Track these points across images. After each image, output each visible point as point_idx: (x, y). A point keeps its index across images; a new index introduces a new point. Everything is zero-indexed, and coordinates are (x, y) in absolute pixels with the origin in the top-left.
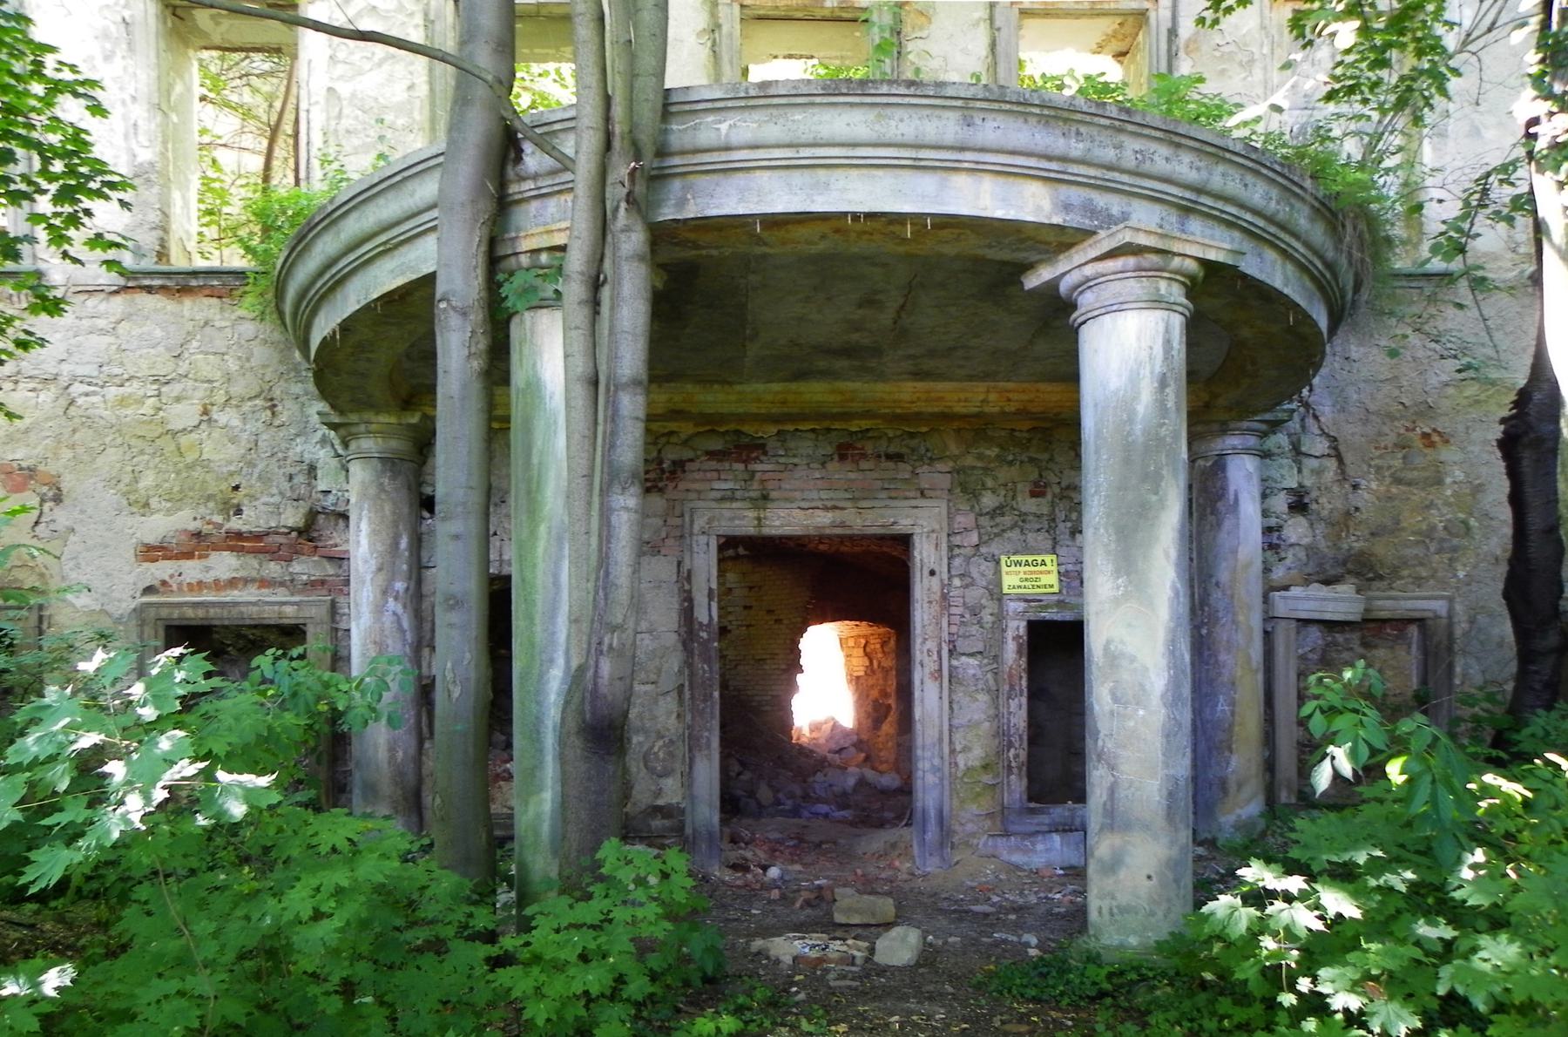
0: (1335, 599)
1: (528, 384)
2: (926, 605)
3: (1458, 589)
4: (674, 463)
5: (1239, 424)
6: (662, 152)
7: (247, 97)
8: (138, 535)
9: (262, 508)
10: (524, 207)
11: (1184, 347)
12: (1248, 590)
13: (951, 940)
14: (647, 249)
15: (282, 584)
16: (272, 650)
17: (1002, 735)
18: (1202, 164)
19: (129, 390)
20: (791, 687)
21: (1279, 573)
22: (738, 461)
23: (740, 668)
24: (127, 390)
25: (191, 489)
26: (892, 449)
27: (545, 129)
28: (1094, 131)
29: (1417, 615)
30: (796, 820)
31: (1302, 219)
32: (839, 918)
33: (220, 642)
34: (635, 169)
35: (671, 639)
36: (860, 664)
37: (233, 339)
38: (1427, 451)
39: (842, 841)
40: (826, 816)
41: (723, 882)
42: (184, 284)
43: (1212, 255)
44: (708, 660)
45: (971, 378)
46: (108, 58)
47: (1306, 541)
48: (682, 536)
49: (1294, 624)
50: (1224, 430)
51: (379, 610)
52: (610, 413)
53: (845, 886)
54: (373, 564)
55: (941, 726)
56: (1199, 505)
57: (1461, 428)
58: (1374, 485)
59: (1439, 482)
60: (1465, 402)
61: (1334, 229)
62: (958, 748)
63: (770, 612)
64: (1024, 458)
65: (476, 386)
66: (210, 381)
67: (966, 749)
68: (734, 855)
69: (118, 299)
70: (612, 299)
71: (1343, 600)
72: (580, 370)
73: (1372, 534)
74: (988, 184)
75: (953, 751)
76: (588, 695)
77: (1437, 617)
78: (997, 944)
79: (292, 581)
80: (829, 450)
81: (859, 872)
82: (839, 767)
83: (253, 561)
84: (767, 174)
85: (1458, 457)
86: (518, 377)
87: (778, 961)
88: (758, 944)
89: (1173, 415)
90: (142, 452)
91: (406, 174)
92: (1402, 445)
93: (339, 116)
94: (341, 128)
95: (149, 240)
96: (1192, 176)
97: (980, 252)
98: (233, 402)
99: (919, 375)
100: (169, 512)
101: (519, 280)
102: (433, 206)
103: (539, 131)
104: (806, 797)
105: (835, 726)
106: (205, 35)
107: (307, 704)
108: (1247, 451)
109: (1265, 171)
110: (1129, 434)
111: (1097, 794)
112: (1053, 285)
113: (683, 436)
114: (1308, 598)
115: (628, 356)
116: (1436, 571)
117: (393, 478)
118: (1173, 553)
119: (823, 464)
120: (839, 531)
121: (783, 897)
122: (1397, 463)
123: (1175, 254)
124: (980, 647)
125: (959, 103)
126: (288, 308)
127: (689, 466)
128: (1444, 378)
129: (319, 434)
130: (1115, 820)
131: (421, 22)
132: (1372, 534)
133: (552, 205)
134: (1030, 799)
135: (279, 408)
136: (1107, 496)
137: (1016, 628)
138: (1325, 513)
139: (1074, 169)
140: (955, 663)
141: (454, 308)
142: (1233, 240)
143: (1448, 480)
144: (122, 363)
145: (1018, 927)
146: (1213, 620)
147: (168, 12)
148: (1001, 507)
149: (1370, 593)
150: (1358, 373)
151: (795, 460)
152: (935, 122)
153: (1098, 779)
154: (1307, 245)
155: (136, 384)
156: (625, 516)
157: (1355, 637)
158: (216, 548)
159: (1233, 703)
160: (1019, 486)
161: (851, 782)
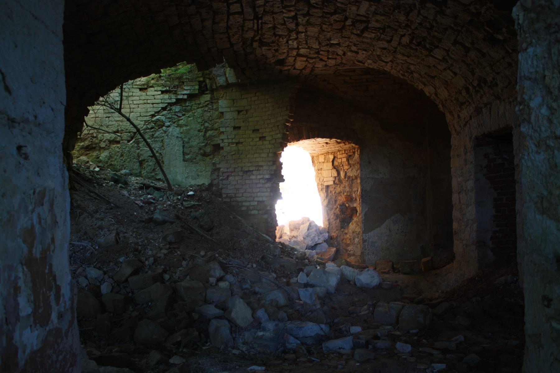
20: (275, 193)
36: (329, 176)
63: (255, 131)
161: (333, 281)
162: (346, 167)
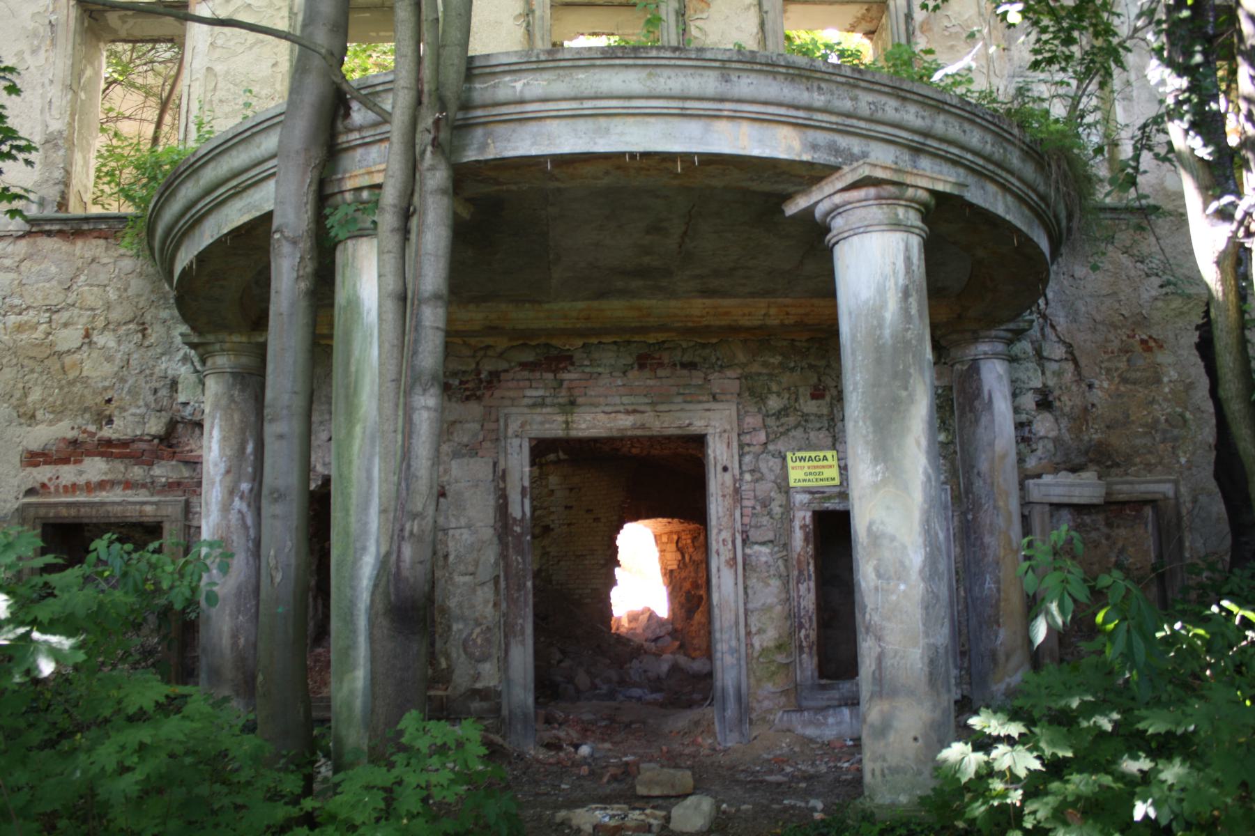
0: (1080, 485)
1: (349, 302)
2: (720, 499)
3: (1181, 473)
4: (491, 373)
5: (988, 333)
6: (466, 106)
7: (151, 80)
8: (24, 443)
9: (130, 418)
10: (351, 153)
11: (923, 263)
12: (1008, 477)
13: (744, 807)
14: (450, 185)
15: (144, 486)
16: (109, 535)
17: (793, 617)
18: (926, 114)
19: (26, 318)
20: (611, 582)
21: (1032, 463)
22: (549, 370)
23: (562, 563)
24: (24, 318)
25: (71, 402)
26: (686, 359)
27: (370, 90)
28: (834, 87)
29: (1149, 497)
30: (608, 703)
31: (1015, 159)
32: (641, 790)
33: (67, 537)
34: (438, 120)
35: (488, 533)
36: (673, 558)
37: (114, 272)
38: (1145, 355)
39: (651, 721)
40: (639, 699)
41: (538, 761)
42: (76, 228)
43: (940, 187)
44: (520, 552)
45: (752, 295)
46: (34, 52)
47: (1052, 434)
48: (497, 439)
49: (1047, 508)
50: (976, 339)
51: (226, 508)
52: (414, 323)
53: (650, 761)
54: (222, 467)
55: (737, 610)
56: (959, 404)
57: (1171, 335)
58: (1105, 384)
59: (1158, 381)
60: (1172, 313)
61: (1042, 168)
62: (754, 630)
63: (589, 511)
64: (804, 364)
65: (303, 304)
66: (92, 309)
67: (761, 631)
68: (548, 735)
69: (23, 242)
70: (418, 226)
71: (1087, 485)
72: (391, 287)
73: (1108, 427)
74: (746, 128)
75: (748, 634)
76: (391, 578)
77: (1166, 498)
78: (786, 809)
79: (153, 483)
80: (629, 360)
81: (664, 748)
82: (654, 654)
83: (120, 466)
84: (556, 122)
85: (1171, 359)
86: (341, 297)
87: (579, 830)
88: (562, 814)
89: (916, 320)
90: (32, 371)
91: (254, 130)
92: (1125, 350)
93: (215, 89)
94: (216, 99)
95: (53, 193)
96: (919, 123)
97: (744, 184)
98: (111, 327)
99: (706, 293)
100: (51, 423)
101: (339, 215)
102: (274, 156)
103: (363, 92)
104: (622, 682)
105: (652, 616)
106: (115, 31)
107: (136, 584)
108: (996, 355)
109: (979, 120)
110: (879, 337)
111: (867, 666)
112: (809, 211)
113: (499, 350)
114: (1057, 485)
115: (431, 274)
116: (1162, 458)
117: (242, 390)
118: (924, 442)
119: (624, 373)
120: (639, 433)
121: (592, 773)
122: (1123, 365)
123: (908, 186)
124: (770, 536)
125: (717, 64)
126: (157, 244)
127: (503, 376)
128: (1154, 293)
129: (181, 353)
130: (883, 687)
131: (287, 14)
132: (1108, 427)
133: (374, 152)
134: (821, 676)
135: (149, 331)
136: (863, 393)
137: (803, 517)
138: (1067, 409)
139: (819, 116)
140: (748, 551)
141: (286, 238)
142: (958, 175)
143: (1165, 380)
144: (21, 296)
145: (808, 793)
146: (976, 506)
147: (86, 16)
148: (785, 409)
149: (1109, 479)
150: (1080, 291)
151: (600, 370)
152: (698, 79)
153: (867, 649)
154: (1020, 179)
155: (31, 313)
156: (425, 414)
157: (1100, 518)
158: (89, 454)
159: (998, 582)
160: (801, 390)
161: (665, 667)
162: (691, 550)
